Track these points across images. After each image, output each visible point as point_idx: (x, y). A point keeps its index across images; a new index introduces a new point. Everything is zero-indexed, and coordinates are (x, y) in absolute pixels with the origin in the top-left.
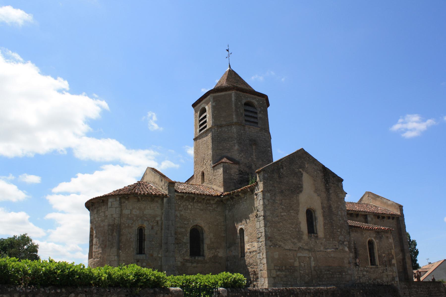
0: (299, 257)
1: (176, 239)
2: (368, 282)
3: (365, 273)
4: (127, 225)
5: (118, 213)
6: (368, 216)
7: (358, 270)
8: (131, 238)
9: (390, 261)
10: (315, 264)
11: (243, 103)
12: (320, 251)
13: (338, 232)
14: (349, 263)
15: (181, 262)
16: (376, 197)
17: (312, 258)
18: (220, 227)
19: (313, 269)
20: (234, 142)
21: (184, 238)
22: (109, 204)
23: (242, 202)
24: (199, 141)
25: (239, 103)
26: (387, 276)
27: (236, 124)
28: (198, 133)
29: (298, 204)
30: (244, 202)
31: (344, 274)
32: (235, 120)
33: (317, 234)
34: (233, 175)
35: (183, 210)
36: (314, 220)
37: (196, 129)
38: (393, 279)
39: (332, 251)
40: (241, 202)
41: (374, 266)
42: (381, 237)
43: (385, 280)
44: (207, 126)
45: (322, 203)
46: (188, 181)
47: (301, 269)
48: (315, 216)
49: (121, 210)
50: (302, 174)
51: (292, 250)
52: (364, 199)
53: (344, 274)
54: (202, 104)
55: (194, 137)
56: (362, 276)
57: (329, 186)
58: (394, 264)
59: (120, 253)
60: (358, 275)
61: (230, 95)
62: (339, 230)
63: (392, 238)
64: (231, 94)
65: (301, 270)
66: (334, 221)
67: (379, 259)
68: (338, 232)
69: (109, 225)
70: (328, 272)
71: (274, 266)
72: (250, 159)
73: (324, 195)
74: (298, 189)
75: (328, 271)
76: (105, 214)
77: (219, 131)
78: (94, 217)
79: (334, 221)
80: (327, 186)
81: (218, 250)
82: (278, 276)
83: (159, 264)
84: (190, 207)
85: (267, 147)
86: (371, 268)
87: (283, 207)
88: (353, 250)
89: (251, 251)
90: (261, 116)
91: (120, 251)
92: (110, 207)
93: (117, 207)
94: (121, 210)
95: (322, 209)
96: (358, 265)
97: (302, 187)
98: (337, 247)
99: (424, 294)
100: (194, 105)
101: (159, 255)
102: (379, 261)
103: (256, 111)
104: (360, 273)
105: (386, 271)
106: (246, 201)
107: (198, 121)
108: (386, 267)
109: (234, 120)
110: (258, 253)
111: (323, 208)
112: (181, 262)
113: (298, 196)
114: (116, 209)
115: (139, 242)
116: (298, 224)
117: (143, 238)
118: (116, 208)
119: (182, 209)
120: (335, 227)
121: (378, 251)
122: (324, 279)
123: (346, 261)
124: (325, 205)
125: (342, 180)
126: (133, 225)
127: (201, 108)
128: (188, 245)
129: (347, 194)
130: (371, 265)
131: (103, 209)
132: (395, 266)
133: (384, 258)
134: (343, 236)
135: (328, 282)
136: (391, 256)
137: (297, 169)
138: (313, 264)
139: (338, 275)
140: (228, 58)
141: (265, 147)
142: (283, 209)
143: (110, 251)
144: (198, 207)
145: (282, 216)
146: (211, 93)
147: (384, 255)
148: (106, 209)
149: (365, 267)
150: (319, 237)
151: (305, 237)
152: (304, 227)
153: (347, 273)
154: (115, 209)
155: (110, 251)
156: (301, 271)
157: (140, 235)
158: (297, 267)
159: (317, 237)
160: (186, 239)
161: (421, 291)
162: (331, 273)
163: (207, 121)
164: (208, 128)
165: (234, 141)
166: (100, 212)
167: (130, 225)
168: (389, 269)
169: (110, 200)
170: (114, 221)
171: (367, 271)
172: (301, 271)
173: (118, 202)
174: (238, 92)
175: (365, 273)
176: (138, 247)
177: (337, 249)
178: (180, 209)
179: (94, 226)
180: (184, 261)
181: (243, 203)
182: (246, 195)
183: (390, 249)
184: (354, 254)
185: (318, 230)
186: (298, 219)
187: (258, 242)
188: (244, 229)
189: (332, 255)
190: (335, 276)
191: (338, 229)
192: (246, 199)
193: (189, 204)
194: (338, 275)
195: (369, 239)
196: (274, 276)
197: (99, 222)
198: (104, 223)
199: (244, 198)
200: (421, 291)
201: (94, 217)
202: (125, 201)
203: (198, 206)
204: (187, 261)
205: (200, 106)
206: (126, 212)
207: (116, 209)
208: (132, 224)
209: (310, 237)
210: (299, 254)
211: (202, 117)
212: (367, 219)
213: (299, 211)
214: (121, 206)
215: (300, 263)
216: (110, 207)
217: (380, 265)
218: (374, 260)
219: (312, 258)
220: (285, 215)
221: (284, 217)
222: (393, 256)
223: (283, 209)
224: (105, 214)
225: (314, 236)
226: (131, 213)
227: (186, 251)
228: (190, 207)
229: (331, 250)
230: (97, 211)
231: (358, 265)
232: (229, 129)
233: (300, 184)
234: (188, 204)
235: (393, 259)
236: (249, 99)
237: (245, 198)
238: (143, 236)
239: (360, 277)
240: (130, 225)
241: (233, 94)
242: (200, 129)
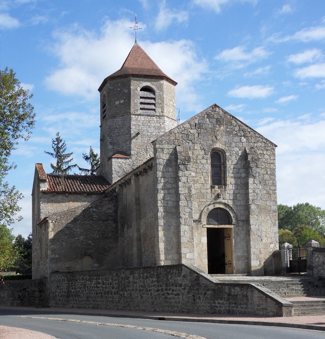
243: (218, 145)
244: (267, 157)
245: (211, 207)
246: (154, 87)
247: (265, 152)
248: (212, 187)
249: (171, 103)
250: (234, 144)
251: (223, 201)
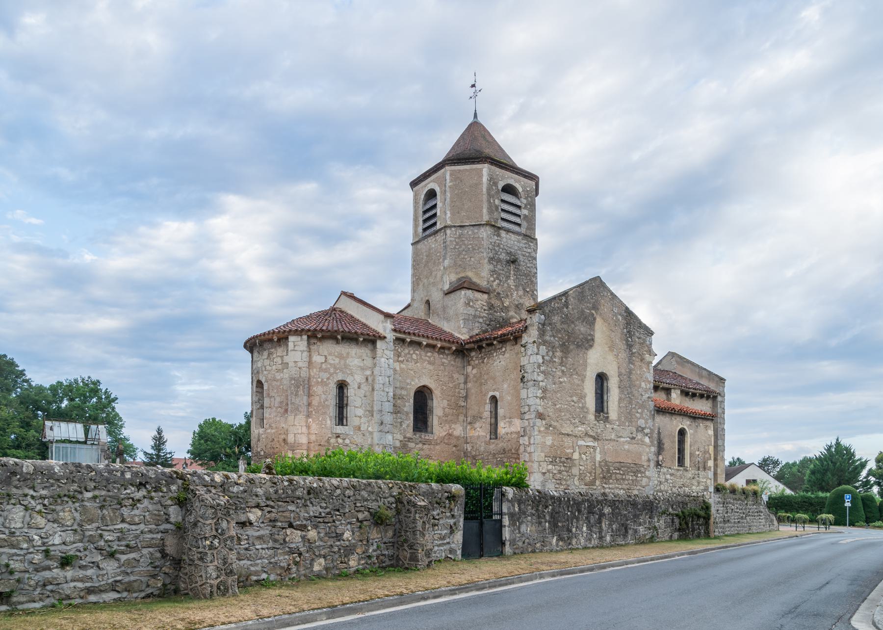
0: (580, 447)
1: (394, 405)
2: (671, 490)
3: (668, 477)
4: (320, 380)
5: (305, 360)
6: (673, 391)
7: (660, 472)
8: (327, 400)
9: (705, 463)
10: (601, 458)
11: (500, 187)
12: (610, 440)
13: (638, 412)
14: (649, 460)
15: (401, 441)
16: (682, 361)
17: (598, 448)
18: (457, 390)
19: (597, 465)
20: (482, 255)
21: (405, 406)
22: (291, 345)
23: (496, 355)
24: (419, 246)
25: (494, 188)
26: (699, 483)
27: (488, 224)
28: (421, 234)
29: (585, 365)
30: (501, 356)
31: (639, 475)
32: (486, 218)
33: (608, 413)
34: (479, 310)
35: (405, 361)
36: (605, 393)
37: (416, 226)
38: (706, 489)
39: (626, 441)
40: (495, 354)
41: (681, 468)
42: (697, 426)
43: (695, 489)
44: (438, 224)
45: (619, 368)
46: (398, 313)
47: (581, 464)
48: (607, 387)
49: (310, 356)
50: (595, 319)
51: (570, 435)
52: (664, 362)
53: (639, 475)
54: (429, 183)
55: (411, 242)
56: (664, 480)
57: (632, 342)
58: (710, 467)
59: (310, 422)
60: (658, 479)
61: (479, 173)
62: (640, 411)
63: (712, 428)
64: (481, 170)
65: (582, 466)
66: (633, 396)
67: (690, 458)
68: (638, 412)
69: (292, 379)
70: (618, 472)
71: (546, 456)
72: (506, 285)
73: (623, 355)
74: (587, 343)
75: (619, 469)
76: (282, 360)
77: (458, 234)
78: (263, 363)
79: (633, 396)
80: (629, 341)
81: (453, 426)
82: (549, 471)
83: (369, 442)
84: (414, 356)
85: (532, 267)
86: (678, 470)
87: (563, 368)
88: (656, 442)
89: (507, 432)
90: (527, 214)
91: (311, 420)
92: (291, 351)
93: (304, 351)
94: (310, 356)
95: (619, 376)
96: (660, 465)
97: (593, 340)
98: (635, 436)
99: (740, 513)
100: (414, 184)
101: (370, 429)
102: (690, 462)
103: (519, 204)
104: (661, 477)
105: (698, 477)
106: (504, 355)
107: (421, 212)
108: (699, 470)
109: (484, 218)
110: (522, 436)
111: (620, 375)
112: (401, 441)
113: (586, 354)
114: (302, 354)
115: (339, 407)
116: (582, 397)
117: (345, 402)
118: (302, 352)
119: (404, 360)
120: (634, 406)
121: (691, 446)
122: (611, 481)
123: (644, 458)
124: (623, 371)
125: (652, 333)
126: (330, 381)
127: (426, 190)
128: (411, 416)
129: (656, 355)
130: (678, 466)
131: (280, 351)
132: (710, 470)
133: (266, 532)
134: (643, 420)
135: (617, 485)
136: (707, 456)
137: (589, 310)
138: (598, 458)
139: (632, 476)
140: (473, 100)
141: (528, 267)
142: (563, 371)
143: (294, 418)
144: (427, 358)
145: (561, 383)
146: (448, 164)
147: (697, 453)
148: (285, 353)
149: (670, 468)
150: (610, 418)
151: (591, 417)
152: (591, 402)
153: (643, 475)
154: (300, 353)
155: (294, 418)
156: (581, 467)
157: (339, 397)
158: (576, 460)
159: (608, 417)
160: (409, 406)
161: (737, 508)
162: (621, 472)
163: (438, 214)
164: (438, 226)
165: (483, 253)
166: (275, 356)
167: (325, 380)
168: (702, 473)
169: (292, 339)
170: (300, 373)
171: (672, 475)
172: (581, 467)
173: (305, 343)
174: (493, 168)
175: (668, 477)
176: (337, 415)
177: (633, 438)
178: (400, 359)
179: (264, 378)
180: (405, 439)
181: (499, 357)
182: (505, 346)
183: (708, 445)
184: (656, 448)
185: (610, 408)
186: (584, 389)
187: (522, 419)
188: (498, 397)
189: (626, 447)
190: (627, 477)
191: (639, 408)
192: (504, 352)
193: (414, 353)
194: (632, 476)
195: (681, 426)
196: (544, 471)
197: (273, 372)
198: (282, 375)
199: (501, 348)
200: (737, 508)
201: (263, 363)
202: (316, 342)
203: (426, 356)
204: (410, 440)
205: (426, 185)
206: (317, 359)
207: (302, 354)
208: (328, 379)
209: (597, 418)
210: (581, 443)
211: (428, 207)
212: (671, 395)
213: (585, 377)
214: (310, 349)
215: (580, 454)
216: (291, 351)
217: (690, 467)
218: (683, 458)
219: (598, 448)
220: (564, 382)
221: (564, 384)
222: (710, 454)
223: (563, 371)
224: (282, 360)
225: (604, 416)
226: (326, 361)
227: (408, 426)
228: (414, 356)
229: (626, 439)
230: (269, 355)
231: (660, 465)
232: (476, 231)
233: (590, 335)
234: (412, 352)
235: (711, 459)
236: (511, 182)
237: (504, 349)
238: (345, 399)
239: (660, 482)
240: (325, 380)
241: (484, 170)
242: (425, 226)
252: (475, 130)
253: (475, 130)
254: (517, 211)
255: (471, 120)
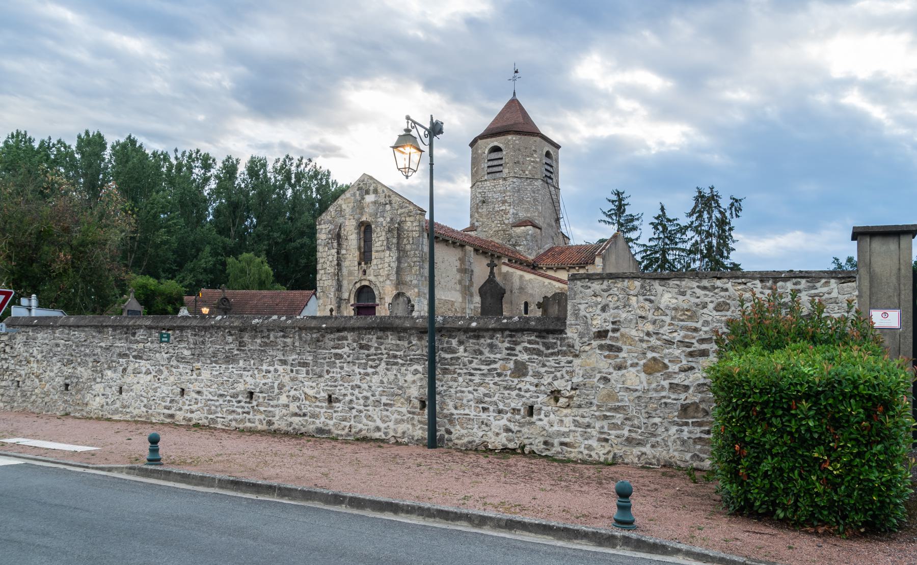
236: (496, 144)
243: (364, 219)
244: (409, 224)
245: (358, 285)
246: (501, 146)
247: (407, 219)
248: (359, 264)
249: (528, 159)
250: (379, 214)
251: (369, 278)
252: (514, 105)
253: (514, 105)
254: (490, 163)
255: (510, 97)
